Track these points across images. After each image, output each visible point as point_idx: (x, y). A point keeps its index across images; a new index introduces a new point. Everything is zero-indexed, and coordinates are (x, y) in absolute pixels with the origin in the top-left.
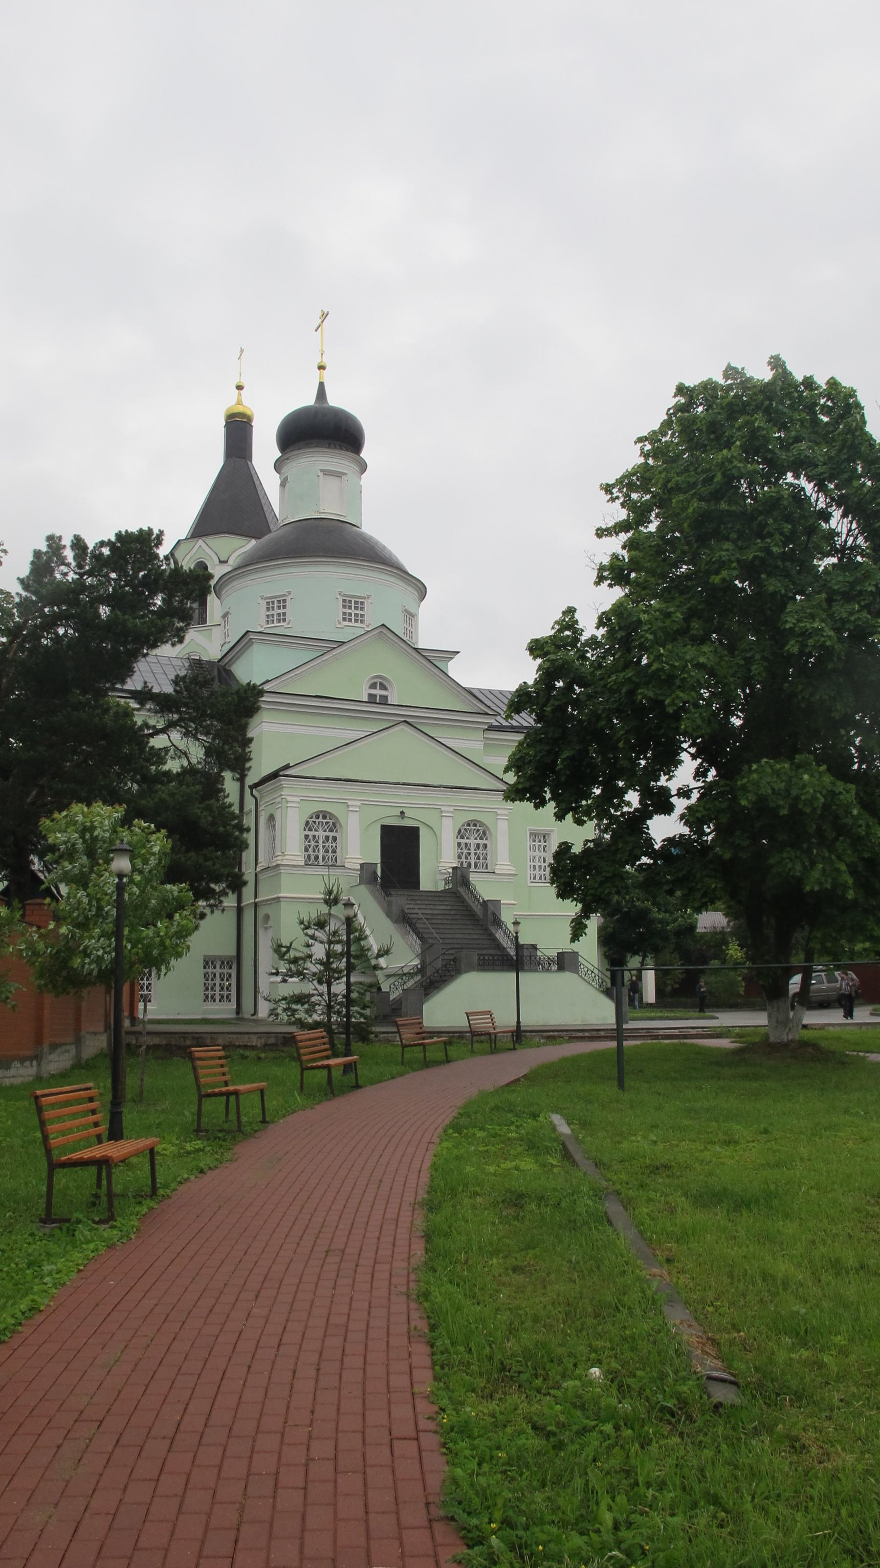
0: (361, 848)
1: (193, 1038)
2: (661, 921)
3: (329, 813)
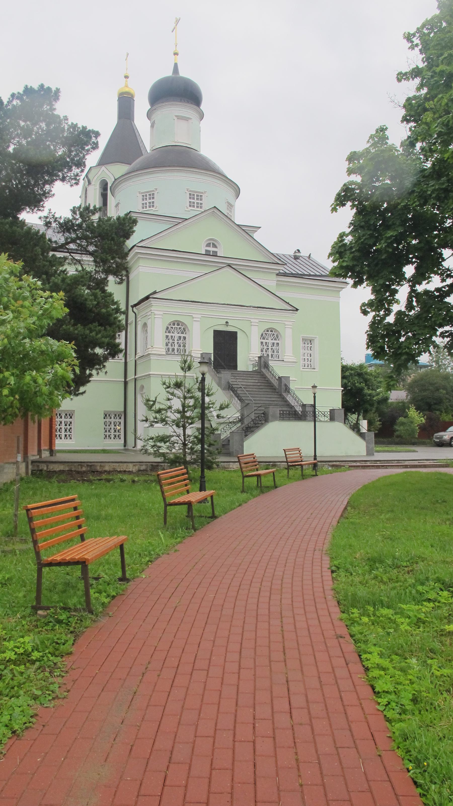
0: (201, 344)
1: (88, 466)
2: (370, 395)
3: (181, 322)
